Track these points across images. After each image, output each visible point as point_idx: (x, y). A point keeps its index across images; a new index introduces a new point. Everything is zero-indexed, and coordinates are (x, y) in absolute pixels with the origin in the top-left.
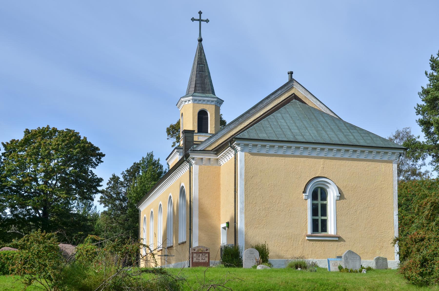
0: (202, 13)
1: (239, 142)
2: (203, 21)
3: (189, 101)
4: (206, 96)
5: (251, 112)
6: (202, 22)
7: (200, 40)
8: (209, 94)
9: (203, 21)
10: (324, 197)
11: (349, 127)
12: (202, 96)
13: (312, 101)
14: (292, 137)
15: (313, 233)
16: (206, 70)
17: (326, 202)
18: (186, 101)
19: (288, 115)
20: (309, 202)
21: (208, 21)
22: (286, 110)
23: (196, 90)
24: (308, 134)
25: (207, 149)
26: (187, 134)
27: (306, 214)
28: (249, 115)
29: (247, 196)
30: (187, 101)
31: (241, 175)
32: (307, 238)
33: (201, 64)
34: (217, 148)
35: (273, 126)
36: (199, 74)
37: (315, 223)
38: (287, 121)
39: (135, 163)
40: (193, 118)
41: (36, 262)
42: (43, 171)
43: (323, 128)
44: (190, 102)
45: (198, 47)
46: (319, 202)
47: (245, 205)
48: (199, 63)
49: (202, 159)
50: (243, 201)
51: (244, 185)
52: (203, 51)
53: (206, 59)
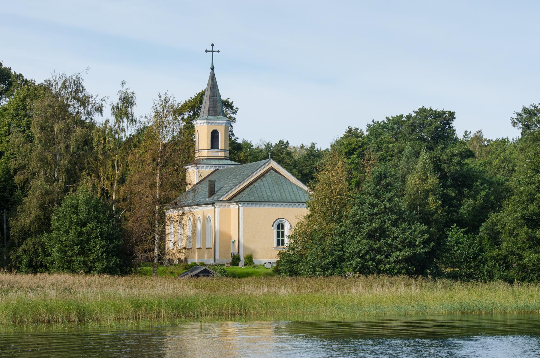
0: (214, 45)
2: (215, 51)
3: (204, 123)
4: (217, 119)
6: (214, 53)
7: (213, 69)
9: (215, 51)
10: (283, 227)
11: (298, 190)
14: (267, 198)
16: (217, 95)
18: (201, 123)
19: (266, 183)
21: (219, 52)
24: (275, 196)
25: (224, 199)
29: (244, 229)
32: (274, 249)
36: (212, 99)
37: (278, 241)
38: (266, 187)
39: (131, 134)
40: (207, 137)
41: (315, 286)
43: (284, 192)
44: (204, 124)
46: (281, 231)
48: (212, 89)
49: (221, 205)
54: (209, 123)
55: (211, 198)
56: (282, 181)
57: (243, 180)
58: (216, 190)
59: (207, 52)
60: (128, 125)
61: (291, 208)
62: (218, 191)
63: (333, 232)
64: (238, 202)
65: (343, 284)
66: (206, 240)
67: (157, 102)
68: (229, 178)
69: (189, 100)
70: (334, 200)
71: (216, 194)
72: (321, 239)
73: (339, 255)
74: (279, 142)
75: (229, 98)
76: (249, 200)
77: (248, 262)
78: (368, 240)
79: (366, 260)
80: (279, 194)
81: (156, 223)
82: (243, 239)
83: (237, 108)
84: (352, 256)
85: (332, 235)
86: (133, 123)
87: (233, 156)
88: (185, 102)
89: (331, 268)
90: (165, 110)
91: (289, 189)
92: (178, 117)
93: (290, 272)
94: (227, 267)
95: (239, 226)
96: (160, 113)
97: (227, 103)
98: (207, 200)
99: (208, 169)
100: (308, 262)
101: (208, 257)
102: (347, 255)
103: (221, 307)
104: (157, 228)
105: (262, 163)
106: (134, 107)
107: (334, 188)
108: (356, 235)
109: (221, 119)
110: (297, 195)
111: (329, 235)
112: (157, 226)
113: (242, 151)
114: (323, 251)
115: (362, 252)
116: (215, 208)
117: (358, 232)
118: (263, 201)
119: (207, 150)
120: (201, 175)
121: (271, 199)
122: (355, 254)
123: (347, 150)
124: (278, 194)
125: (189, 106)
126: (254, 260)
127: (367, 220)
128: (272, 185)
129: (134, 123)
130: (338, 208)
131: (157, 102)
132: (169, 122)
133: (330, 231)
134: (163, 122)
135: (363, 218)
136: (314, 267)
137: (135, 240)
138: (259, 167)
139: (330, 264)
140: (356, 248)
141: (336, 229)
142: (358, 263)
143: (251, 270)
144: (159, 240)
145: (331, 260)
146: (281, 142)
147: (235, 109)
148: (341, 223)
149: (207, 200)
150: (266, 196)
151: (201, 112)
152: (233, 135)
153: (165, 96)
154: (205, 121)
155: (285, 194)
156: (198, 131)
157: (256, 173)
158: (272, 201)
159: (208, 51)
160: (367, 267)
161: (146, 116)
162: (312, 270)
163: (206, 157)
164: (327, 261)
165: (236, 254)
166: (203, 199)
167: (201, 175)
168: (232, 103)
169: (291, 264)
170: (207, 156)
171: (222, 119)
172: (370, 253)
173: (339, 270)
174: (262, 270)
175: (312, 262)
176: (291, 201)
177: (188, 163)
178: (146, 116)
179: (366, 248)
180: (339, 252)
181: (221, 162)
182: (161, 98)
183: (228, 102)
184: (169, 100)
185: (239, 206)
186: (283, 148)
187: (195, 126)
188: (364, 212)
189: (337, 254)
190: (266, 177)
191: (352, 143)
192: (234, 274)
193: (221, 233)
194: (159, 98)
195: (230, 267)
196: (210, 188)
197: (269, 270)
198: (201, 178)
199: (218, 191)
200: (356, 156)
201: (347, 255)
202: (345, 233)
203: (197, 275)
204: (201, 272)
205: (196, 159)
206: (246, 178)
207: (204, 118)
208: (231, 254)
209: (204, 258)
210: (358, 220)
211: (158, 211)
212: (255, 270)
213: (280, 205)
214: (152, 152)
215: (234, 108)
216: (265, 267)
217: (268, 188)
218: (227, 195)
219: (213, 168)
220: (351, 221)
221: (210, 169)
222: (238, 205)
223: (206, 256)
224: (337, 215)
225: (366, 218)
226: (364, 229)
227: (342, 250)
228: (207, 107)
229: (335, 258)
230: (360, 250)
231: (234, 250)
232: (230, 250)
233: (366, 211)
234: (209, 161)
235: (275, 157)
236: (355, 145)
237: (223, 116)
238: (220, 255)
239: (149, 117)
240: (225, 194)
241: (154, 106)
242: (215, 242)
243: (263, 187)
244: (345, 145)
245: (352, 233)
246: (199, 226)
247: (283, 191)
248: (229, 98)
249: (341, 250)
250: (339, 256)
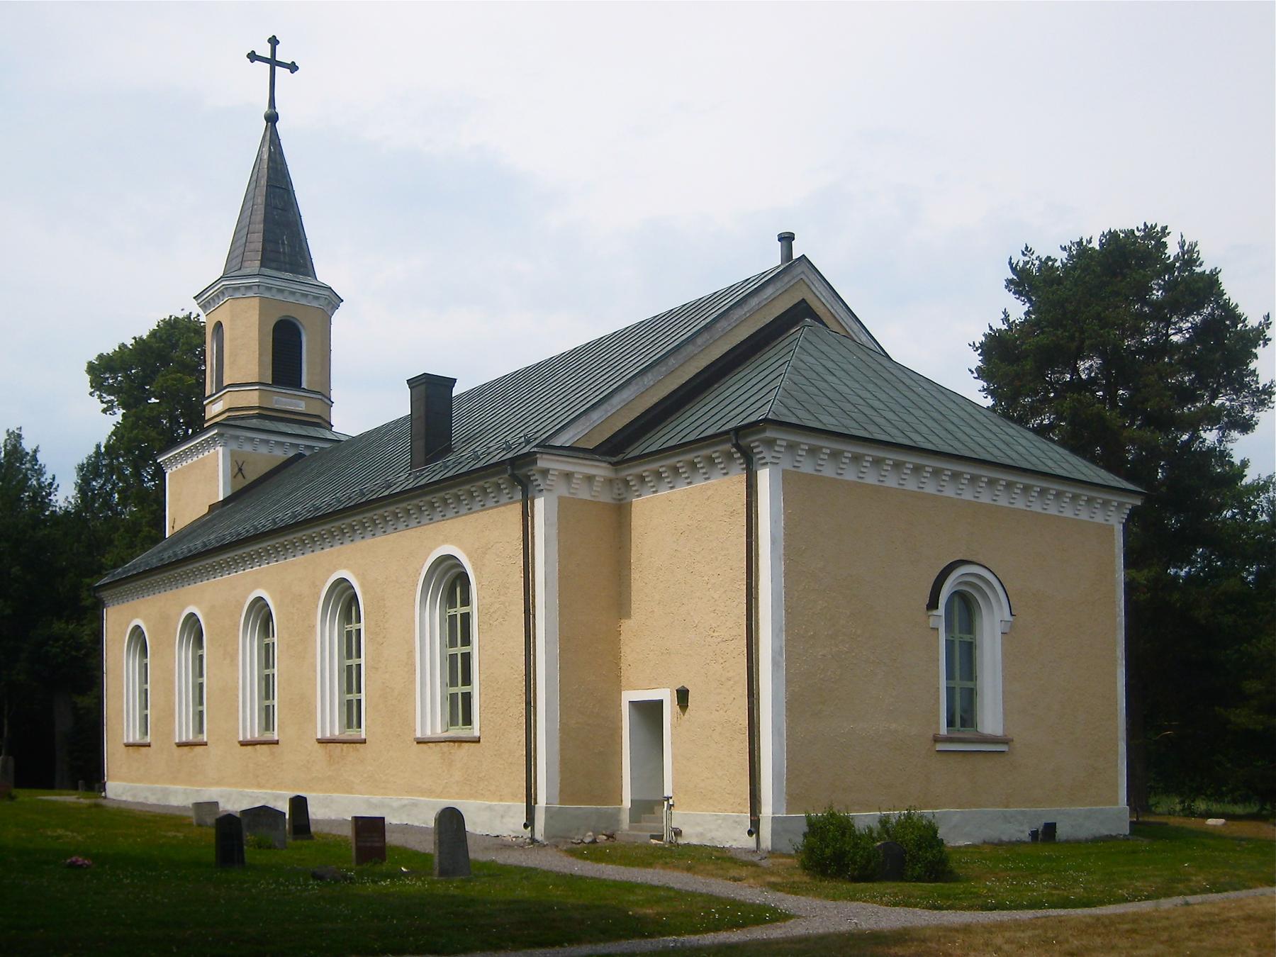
5: (700, 341)
7: (272, 118)
17: (972, 636)
28: (694, 348)
30: (242, 289)
42: (39, 484)
50: (781, 627)
51: (783, 575)
59: (270, 41)
120: (240, 470)
167: (240, 470)
170: (259, 408)
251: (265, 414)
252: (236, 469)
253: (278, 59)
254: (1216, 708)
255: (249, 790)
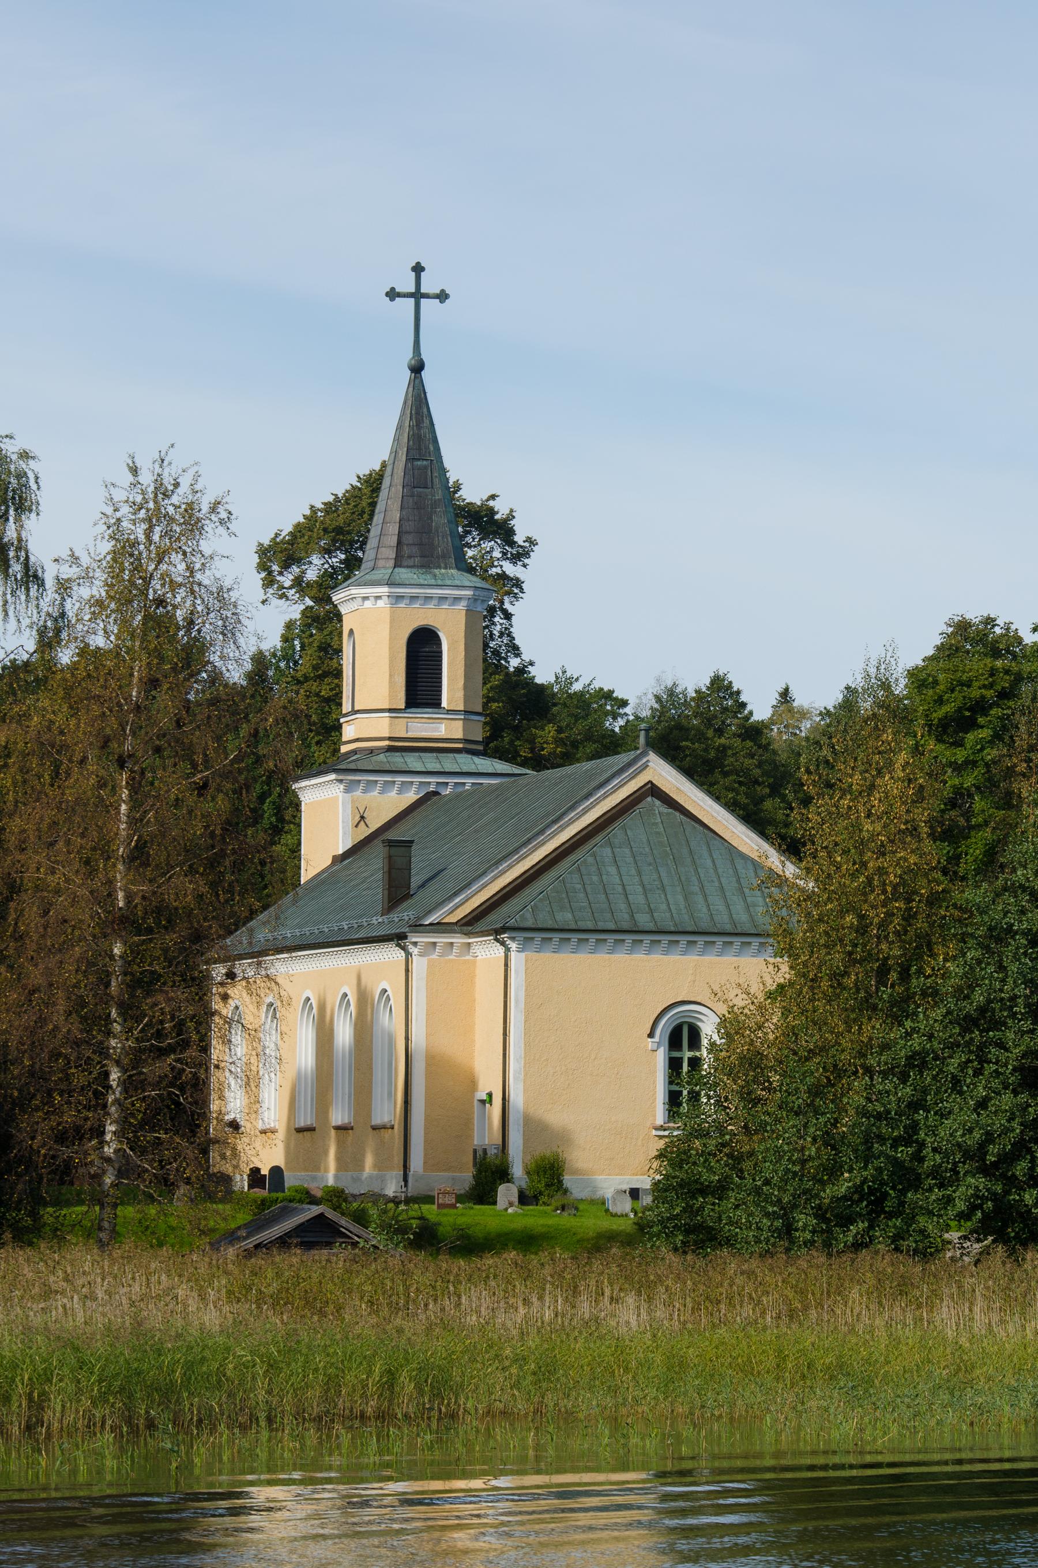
0: (423, 269)
1: (513, 935)
2: (427, 296)
4: (433, 582)
7: (417, 368)
8: (446, 568)
9: (427, 296)
12: (422, 582)
13: (693, 798)
14: (626, 916)
15: (669, 1122)
16: (436, 481)
19: (627, 851)
20: (661, 1058)
22: (626, 834)
23: (402, 557)
24: (664, 907)
25: (445, 921)
26: (394, 850)
27: (654, 1082)
29: (528, 1045)
30: (372, 599)
31: (517, 1001)
32: (654, 1132)
33: (419, 460)
34: (469, 917)
35: (589, 888)
36: (412, 496)
38: (623, 870)
43: (702, 888)
44: (381, 603)
45: (410, 395)
47: (525, 1064)
49: (435, 944)
52: (425, 410)
53: (443, 453)
54: (399, 598)
55: (395, 916)
56: (693, 844)
57: (529, 841)
58: (415, 881)
59: (392, 299)
60: (9, 596)
61: (709, 959)
62: (423, 886)
63: (872, 1061)
64: (504, 929)
65: (904, 1287)
66: (370, 1092)
67: (119, 495)
68: (476, 831)
69: (325, 504)
70: (876, 920)
71: (416, 898)
72: (816, 1091)
73: (896, 1159)
74: (713, 682)
75: (493, 497)
76: (550, 924)
77: (541, 1186)
78: (1023, 1098)
79: (1011, 1182)
80: (680, 898)
81: (114, 1013)
82: (525, 1091)
83: (529, 540)
84: (955, 1164)
85: (869, 1071)
86: (28, 590)
87: (512, 742)
88: (308, 512)
89: (860, 1215)
90: (157, 529)
91: (723, 880)
92: (281, 573)
93: (688, 1231)
94: (440, 1206)
95: (505, 1034)
96: (135, 543)
97: (486, 516)
98: (379, 922)
99: (393, 794)
100: (760, 1188)
101: (378, 1165)
102: (932, 1160)
103: (332, 1384)
104: (115, 1037)
105: (611, 766)
106: (31, 522)
107: (881, 871)
108: (971, 1072)
109: (449, 582)
110: (755, 905)
111: (855, 1073)
112: (117, 1028)
113: (550, 722)
114: (828, 1140)
115: (993, 1149)
116: (408, 955)
117: (981, 1062)
118: (612, 927)
119: (390, 710)
120: (362, 817)
121: (643, 920)
122: (967, 1155)
123: (947, 709)
124: (677, 899)
125: (325, 530)
126: (568, 1180)
127: (1020, 1009)
128: (650, 859)
129: (33, 592)
130: (895, 957)
131: (119, 495)
132: (171, 581)
133: (862, 1055)
134: (147, 581)
135: (1002, 999)
136: (786, 1213)
137: (20, 1091)
138: (596, 783)
139: (856, 1197)
140: (970, 1131)
141: (885, 1047)
142: (978, 1197)
143: (542, 1221)
144: (126, 1090)
145: (863, 1182)
146: (719, 685)
147: (521, 543)
148: (908, 1024)
149: (379, 922)
150: (623, 906)
151: (368, 555)
152: (515, 650)
153: (158, 470)
154: (384, 590)
155: (706, 900)
156: (351, 632)
157: (586, 811)
158: (651, 926)
159: (400, 295)
160: (1021, 1215)
161: (72, 555)
162: (778, 1223)
163: (387, 743)
164: (843, 1188)
165: (492, 1152)
166: (361, 917)
167: (362, 817)
168: (511, 516)
169: (694, 1198)
170: (390, 739)
171: (458, 583)
172: (1029, 1151)
173: (895, 1226)
174: (591, 1224)
175: (780, 1188)
176: (729, 928)
177: (309, 768)
178: (72, 555)
179: (1013, 1130)
180: (894, 1146)
181: (449, 763)
182: (141, 479)
183: (492, 512)
184: (177, 485)
185: (508, 950)
186: (725, 710)
187: (343, 610)
188: (1007, 976)
189: (887, 1157)
190: (624, 829)
191: (971, 681)
192: (468, 1237)
193: (433, 1060)
194: (130, 478)
195: (453, 1206)
196: (390, 872)
197: (621, 1221)
198: (364, 832)
199: (423, 886)
200: (985, 733)
201: (932, 1160)
202: (923, 1066)
203: (283, 1242)
204: (300, 1230)
205: (344, 749)
206: (542, 832)
207: (377, 575)
208: (475, 1151)
209: (361, 1167)
210: (982, 1010)
211: (120, 963)
212: (564, 1220)
213: (683, 944)
214: (96, 709)
215: (516, 538)
216: (607, 1211)
217: (633, 872)
218: (457, 900)
219: (414, 788)
220: (949, 1012)
221: (400, 792)
222: (503, 943)
223: (369, 1160)
224: (893, 986)
225: (1013, 998)
226: (1007, 1050)
227: (911, 1136)
228: (393, 529)
229: (879, 1170)
230: (989, 1138)
231: (488, 1135)
232: (471, 1137)
233: (1014, 968)
234: (398, 760)
235: (687, 747)
236: (984, 686)
237: (459, 569)
238: (425, 1155)
239: (85, 561)
240: (450, 898)
241: (109, 511)
242: (407, 1102)
243: (612, 870)
244: (942, 687)
245: (953, 1065)
246: (344, 1034)
247: (696, 888)
248: (493, 497)
249: (906, 1140)
250: (896, 1162)
251: (397, 747)
252: (358, 818)
253: (413, 290)
254: (121, 904)
255: (838, 1504)
